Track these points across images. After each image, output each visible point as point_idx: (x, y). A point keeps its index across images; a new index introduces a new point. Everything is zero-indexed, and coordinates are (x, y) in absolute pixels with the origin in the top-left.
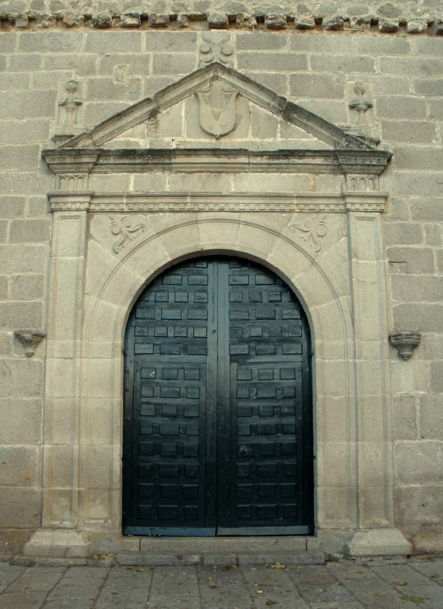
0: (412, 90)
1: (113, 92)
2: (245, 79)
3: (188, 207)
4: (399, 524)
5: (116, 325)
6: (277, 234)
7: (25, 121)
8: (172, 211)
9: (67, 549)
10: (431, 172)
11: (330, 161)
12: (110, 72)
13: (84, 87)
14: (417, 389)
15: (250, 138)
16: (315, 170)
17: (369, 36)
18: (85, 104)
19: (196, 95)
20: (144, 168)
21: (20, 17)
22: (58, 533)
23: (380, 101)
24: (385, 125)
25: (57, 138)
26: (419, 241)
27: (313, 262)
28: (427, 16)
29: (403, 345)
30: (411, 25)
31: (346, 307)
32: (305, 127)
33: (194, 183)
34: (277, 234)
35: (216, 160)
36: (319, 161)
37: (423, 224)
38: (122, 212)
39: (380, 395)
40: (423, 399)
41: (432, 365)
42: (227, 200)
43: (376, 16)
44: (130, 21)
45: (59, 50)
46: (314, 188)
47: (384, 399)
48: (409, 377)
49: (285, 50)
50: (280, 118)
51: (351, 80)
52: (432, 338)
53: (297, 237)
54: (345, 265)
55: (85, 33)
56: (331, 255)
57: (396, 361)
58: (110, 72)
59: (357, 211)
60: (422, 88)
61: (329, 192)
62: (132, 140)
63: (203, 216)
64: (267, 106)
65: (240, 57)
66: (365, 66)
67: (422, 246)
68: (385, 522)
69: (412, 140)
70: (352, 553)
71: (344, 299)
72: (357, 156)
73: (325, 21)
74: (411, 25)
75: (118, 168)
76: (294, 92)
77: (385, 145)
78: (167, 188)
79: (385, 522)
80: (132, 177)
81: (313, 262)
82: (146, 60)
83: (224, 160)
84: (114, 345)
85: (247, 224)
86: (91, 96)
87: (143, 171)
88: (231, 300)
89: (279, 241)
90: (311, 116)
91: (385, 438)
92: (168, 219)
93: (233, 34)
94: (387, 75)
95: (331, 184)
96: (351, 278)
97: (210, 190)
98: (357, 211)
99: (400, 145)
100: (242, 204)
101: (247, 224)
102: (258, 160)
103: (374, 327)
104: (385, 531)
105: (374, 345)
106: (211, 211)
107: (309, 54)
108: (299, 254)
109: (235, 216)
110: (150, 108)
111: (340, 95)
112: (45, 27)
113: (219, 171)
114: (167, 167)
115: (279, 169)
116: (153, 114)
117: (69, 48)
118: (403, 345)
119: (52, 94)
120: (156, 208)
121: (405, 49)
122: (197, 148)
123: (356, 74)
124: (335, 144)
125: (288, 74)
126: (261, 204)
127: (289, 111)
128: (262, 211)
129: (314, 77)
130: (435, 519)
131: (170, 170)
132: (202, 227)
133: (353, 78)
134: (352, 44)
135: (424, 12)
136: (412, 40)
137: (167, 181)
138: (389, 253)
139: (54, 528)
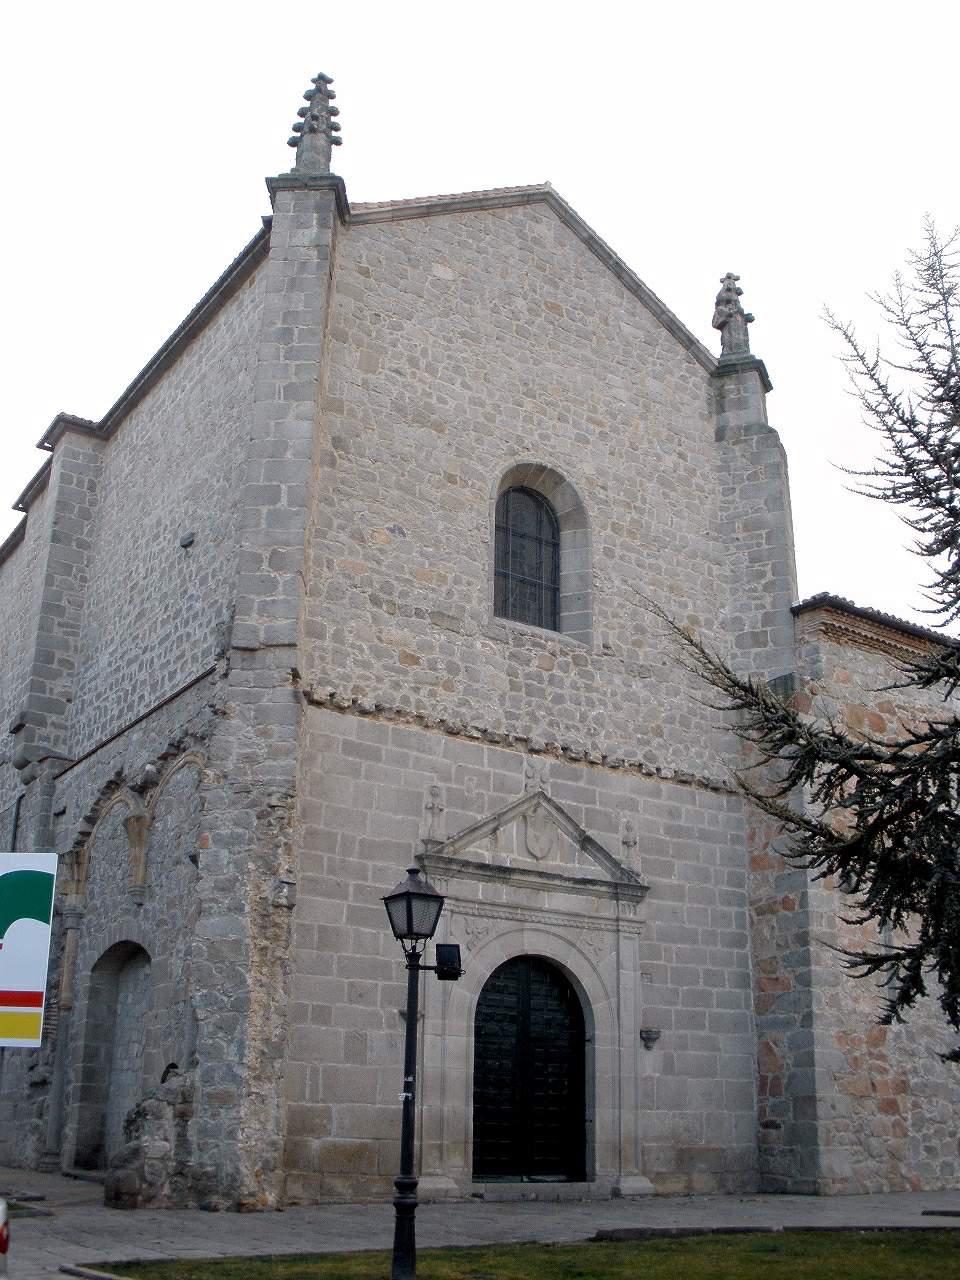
0: (662, 831)
1: (465, 803)
2: (559, 809)
3: (518, 917)
4: (644, 1173)
5: (470, 1009)
6: (573, 945)
7: (399, 817)
8: (507, 919)
9: (447, 1191)
10: (670, 903)
11: (611, 890)
12: (463, 783)
13: (444, 794)
14: (654, 1072)
15: (558, 862)
16: (599, 896)
17: (636, 779)
18: (446, 810)
19: (525, 817)
20: (490, 879)
21: (391, 709)
22: (436, 1179)
23: (641, 839)
24: (644, 861)
25: (426, 842)
26: (660, 959)
27: (595, 969)
28: (673, 766)
29: (648, 1038)
30: (664, 773)
31: (614, 1006)
32: (595, 857)
33: (522, 897)
34: (573, 945)
35: (539, 880)
36: (604, 889)
37: (663, 945)
38: (474, 915)
39: (633, 1075)
40: (658, 1079)
41: (665, 1055)
42: (545, 914)
43: (643, 761)
44: (476, 734)
45: (423, 751)
46: (597, 911)
47: (636, 1078)
48: (650, 1062)
49: (581, 784)
50: (578, 847)
51: (625, 817)
52: (665, 1033)
53: (586, 949)
54: (615, 974)
55: (437, 736)
56: (606, 963)
57: (642, 1050)
58: (463, 783)
59: (625, 931)
60: (669, 830)
61: (607, 914)
62: (480, 851)
63: (528, 925)
64: (569, 834)
65: (554, 785)
66: (632, 806)
67: (662, 962)
68: (636, 1171)
69: (659, 875)
70: (623, 1192)
71: (613, 1000)
72: (626, 887)
73: (609, 760)
74: (664, 773)
75: (472, 876)
76: (589, 825)
77: (644, 880)
78: (504, 899)
79: (636, 1171)
80: (481, 885)
81: (595, 969)
82: (487, 775)
83: (545, 881)
84: (469, 1027)
85: (554, 935)
86: (450, 804)
87: (489, 881)
88: (434, 907)
89: (574, 950)
90: (600, 849)
91: (636, 1108)
92: (504, 925)
93: (549, 760)
94: (647, 816)
95: (608, 909)
96: (618, 984)
97: (525, 903)
98: (625, 931)
99: (654, 879)
100: (554, 918)
101: (554, 935)
102: (567, 884)
103: (631, 1025)
104: (637, 1178)
105: (631, 1038)
106: (533, 922)
107: (598, 790)
108: (586, 963)
109: (548, 928)
110: (492, 826)
111: (616, 831)
112: (408, 722)
113: (539, 888)
114: (505, 881)
115: (578, 892)
116: (495, 830)
117: (431, 751)
118: (648, 1038)
119: (419, 795)
120: (496, 915)
121: (657, 794)
122: (165, 383)
123: (627, 812)
124: (613, 874)
125: (584, 806)
126: (560, 920)
127: (586, 842)
128: (565, 925)
129: (600, 812)
130: (664, 1170)
131: (507, 883)
132: (526, 934)
133: (625, 817)
134: (624, 784)
135: (673, 761)
136: (665, 786)
137: (504, 893)
138: (642, 966)
139: (430, 1175)
